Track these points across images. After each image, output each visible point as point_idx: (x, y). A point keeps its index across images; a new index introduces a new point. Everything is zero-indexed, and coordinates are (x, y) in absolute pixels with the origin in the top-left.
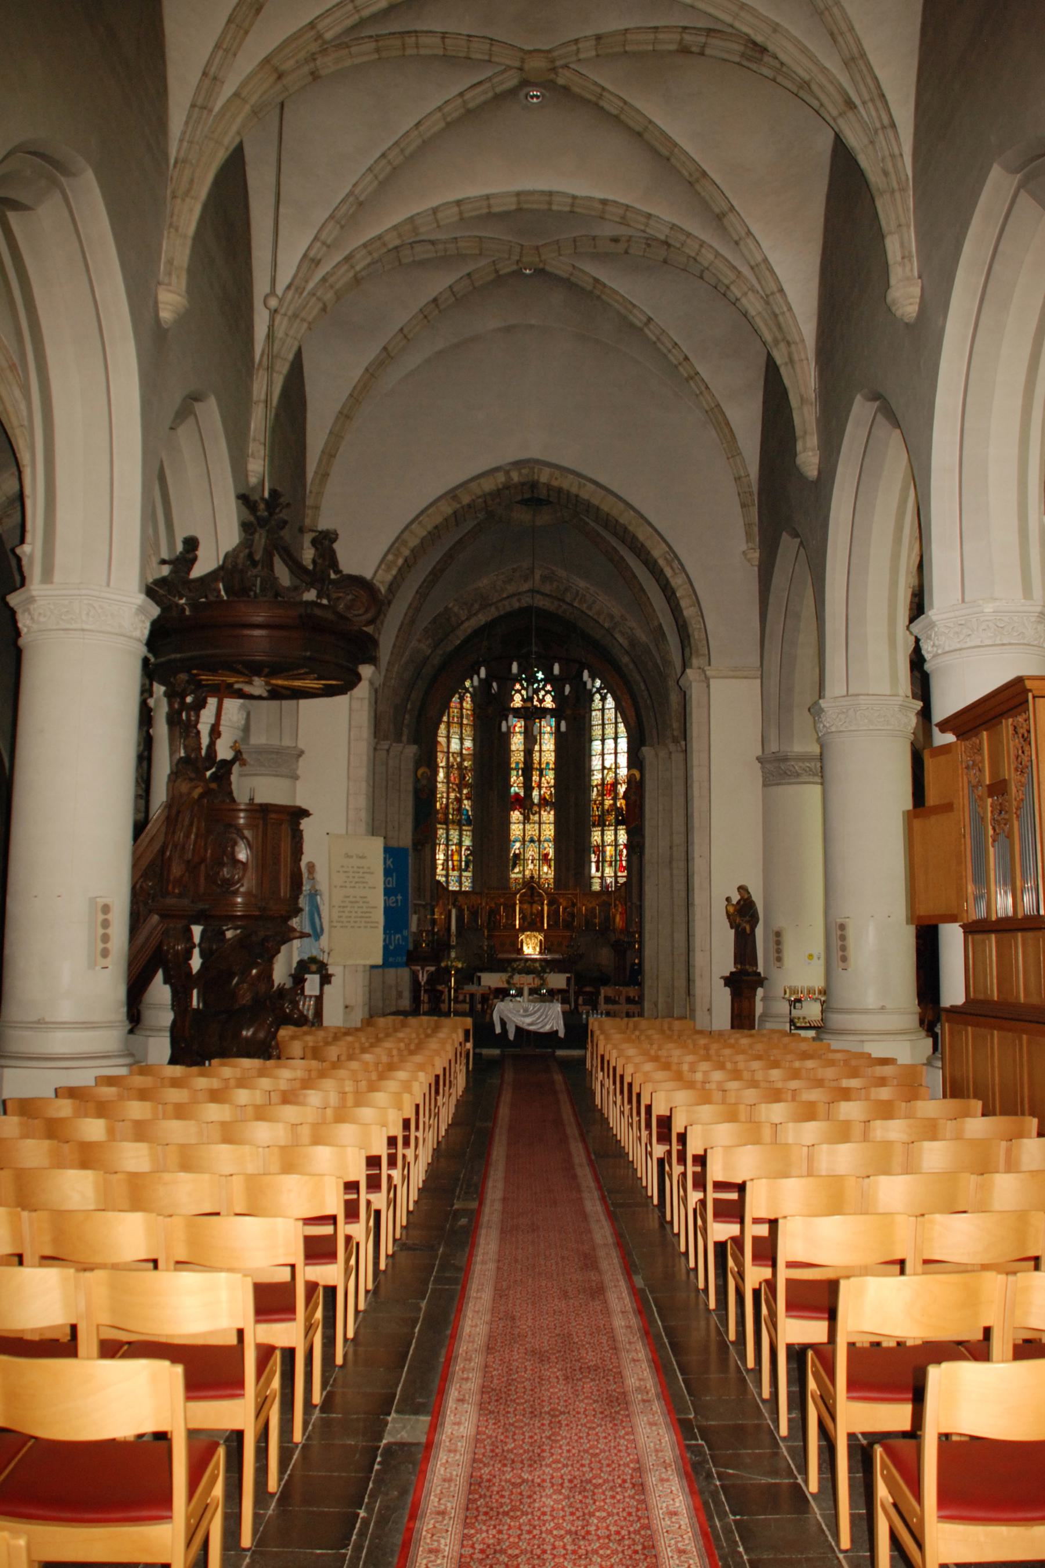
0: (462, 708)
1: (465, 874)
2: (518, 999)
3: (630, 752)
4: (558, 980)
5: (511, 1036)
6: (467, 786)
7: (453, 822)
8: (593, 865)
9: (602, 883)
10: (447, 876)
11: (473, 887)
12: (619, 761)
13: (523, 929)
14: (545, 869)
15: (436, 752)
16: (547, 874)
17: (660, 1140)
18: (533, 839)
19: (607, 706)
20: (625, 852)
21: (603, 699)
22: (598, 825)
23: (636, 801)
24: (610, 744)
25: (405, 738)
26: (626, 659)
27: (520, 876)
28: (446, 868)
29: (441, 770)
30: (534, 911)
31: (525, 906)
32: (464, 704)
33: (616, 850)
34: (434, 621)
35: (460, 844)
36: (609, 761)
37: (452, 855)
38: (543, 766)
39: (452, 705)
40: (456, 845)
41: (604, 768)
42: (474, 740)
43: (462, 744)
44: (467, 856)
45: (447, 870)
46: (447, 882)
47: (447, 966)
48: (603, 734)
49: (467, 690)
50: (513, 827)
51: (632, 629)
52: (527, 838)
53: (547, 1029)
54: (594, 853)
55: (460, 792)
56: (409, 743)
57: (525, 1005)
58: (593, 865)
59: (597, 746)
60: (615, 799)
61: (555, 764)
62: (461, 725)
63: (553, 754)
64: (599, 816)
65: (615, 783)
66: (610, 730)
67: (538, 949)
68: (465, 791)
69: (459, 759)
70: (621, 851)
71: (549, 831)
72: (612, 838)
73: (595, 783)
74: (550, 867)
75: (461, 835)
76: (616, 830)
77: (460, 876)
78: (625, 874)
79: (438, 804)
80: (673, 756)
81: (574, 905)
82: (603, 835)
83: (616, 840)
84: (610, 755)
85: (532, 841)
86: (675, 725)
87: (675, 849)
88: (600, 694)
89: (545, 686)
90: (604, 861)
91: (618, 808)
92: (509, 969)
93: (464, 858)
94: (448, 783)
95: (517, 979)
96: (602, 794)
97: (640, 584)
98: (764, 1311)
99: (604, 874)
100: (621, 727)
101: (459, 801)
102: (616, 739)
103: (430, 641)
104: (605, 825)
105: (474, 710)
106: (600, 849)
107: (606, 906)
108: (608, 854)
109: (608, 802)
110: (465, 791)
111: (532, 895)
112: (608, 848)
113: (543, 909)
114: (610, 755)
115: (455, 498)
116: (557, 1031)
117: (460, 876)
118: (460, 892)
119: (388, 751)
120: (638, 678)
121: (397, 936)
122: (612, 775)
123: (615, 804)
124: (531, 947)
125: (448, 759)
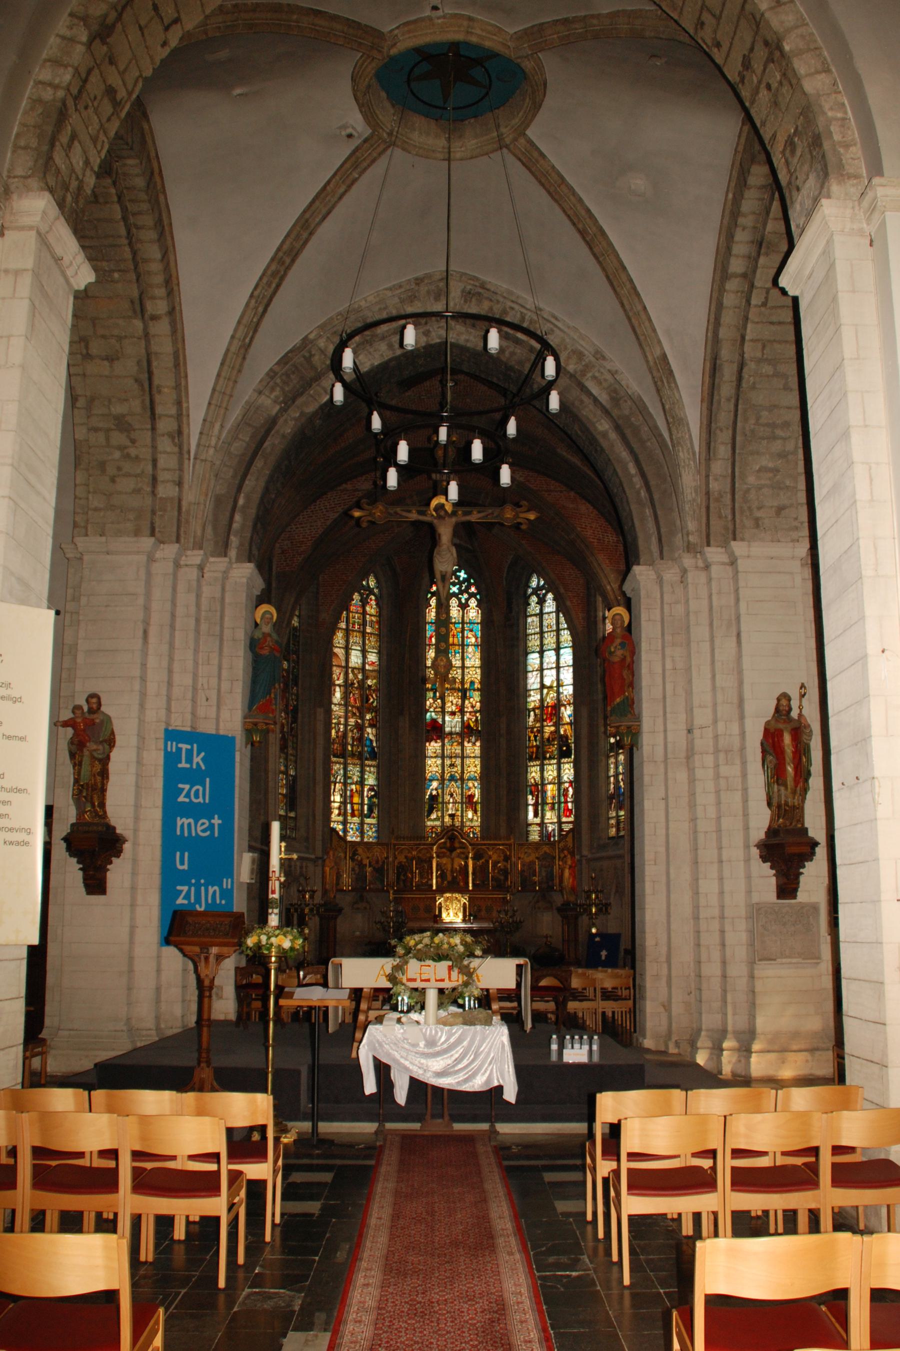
0: (364, 613)
1: (368, 821)
2: (414, 1016)
4: (498, 973)
5: (401, 1095)
6: (369, 710)
7: (353, 755)
8: (531, 809)
9: (541, 832)
10: (345, 823)
11: (378, 838)
12: (562, 677)
13: (441, 891)
14: (470, 814)
15: (331, 666)
16: (471, 820)
17: (606, 1154)
18: (453, 769)
19: (546, 610)
20: (571, 791)
21: (541, 602)
22: (537, 759)
23: (624, 659)
24: (550, 657)
25: (233, 553)
26: (603, 426)
27: (438, 823)
28: (343, 813)
29: (338, 689)
30: (456, 866)
31: (444, 861)
32: (368, 609)
33: (559, 789)
34: (284, 360)
35: (362, 783)
36: (550, 678)
37: (352, 796)
38: (467, 686)
39: (352, 608)
40: (356, 783)
41: (543, 686)
42: (379, 653)
43: (364, 657)
44: (370, 798)
45: (345, 815)
46: (345, 831)
47: (259, 946)
48: (542, 645)
49: (371, 592)
50: (429, 762)
51: (613, 373)
52: (447, 776)
53: (478, 1084)
54: (532, 793)
55: (362, 717)
56: (239, 560)
57: (431, 1029)
59: (533, 659)
60: (557, 725)
61: (480, 683)
62: (364, 634)
63: (479, 671)
64: (537, 746)
65: (558, 705)
66: (550, 640)
67: (461, 915)
68: (368, 717)
69: (360, 676)
70: (566, 790)
71: (474, 767)
72: (556, 775)
73: (532, 706)
74: (475, 812)
75: (362, 772)
76: (559, 764)
77: (362, 824)
78: (571, 819)
79: (333, 732)
80: (690, 576)
81: (507, 859)
82: (542, 771)
83: (559, 776)
84: (551, 670)
85: (452, 778)
86: (691, 525)
87: (697, 733)
88: (538, 596)
89: (468, 587)
90: (544, 803)
91: (561, 737)
92: (400, 950)
93: (366, 801)
94: (346, 705)
95: (414, 967)
96: (540, 719)
97: (631, 281)
99: (544, 820)
100: (566, 636)
101: (360, 728)
102: (557, 650)
103: (277, 392)
104: (545, 758)
105: (380, 615)
106: (539, 789)
107: (547, 860)
108: (549, 794)
109: (549, 729)
110: (368, 717)
111: (452, 843)
112: (549, 787)
113: (467, 865)
114: (551, 670)
116: (499, 1089)
117: (362, 824)
118: (362, 843)
119: (201, 568)
120: (625, 455)
121: (211, 890)
122: (553, 694)
123: (557, 731)
124: (453, 913)
125: (346, 674)
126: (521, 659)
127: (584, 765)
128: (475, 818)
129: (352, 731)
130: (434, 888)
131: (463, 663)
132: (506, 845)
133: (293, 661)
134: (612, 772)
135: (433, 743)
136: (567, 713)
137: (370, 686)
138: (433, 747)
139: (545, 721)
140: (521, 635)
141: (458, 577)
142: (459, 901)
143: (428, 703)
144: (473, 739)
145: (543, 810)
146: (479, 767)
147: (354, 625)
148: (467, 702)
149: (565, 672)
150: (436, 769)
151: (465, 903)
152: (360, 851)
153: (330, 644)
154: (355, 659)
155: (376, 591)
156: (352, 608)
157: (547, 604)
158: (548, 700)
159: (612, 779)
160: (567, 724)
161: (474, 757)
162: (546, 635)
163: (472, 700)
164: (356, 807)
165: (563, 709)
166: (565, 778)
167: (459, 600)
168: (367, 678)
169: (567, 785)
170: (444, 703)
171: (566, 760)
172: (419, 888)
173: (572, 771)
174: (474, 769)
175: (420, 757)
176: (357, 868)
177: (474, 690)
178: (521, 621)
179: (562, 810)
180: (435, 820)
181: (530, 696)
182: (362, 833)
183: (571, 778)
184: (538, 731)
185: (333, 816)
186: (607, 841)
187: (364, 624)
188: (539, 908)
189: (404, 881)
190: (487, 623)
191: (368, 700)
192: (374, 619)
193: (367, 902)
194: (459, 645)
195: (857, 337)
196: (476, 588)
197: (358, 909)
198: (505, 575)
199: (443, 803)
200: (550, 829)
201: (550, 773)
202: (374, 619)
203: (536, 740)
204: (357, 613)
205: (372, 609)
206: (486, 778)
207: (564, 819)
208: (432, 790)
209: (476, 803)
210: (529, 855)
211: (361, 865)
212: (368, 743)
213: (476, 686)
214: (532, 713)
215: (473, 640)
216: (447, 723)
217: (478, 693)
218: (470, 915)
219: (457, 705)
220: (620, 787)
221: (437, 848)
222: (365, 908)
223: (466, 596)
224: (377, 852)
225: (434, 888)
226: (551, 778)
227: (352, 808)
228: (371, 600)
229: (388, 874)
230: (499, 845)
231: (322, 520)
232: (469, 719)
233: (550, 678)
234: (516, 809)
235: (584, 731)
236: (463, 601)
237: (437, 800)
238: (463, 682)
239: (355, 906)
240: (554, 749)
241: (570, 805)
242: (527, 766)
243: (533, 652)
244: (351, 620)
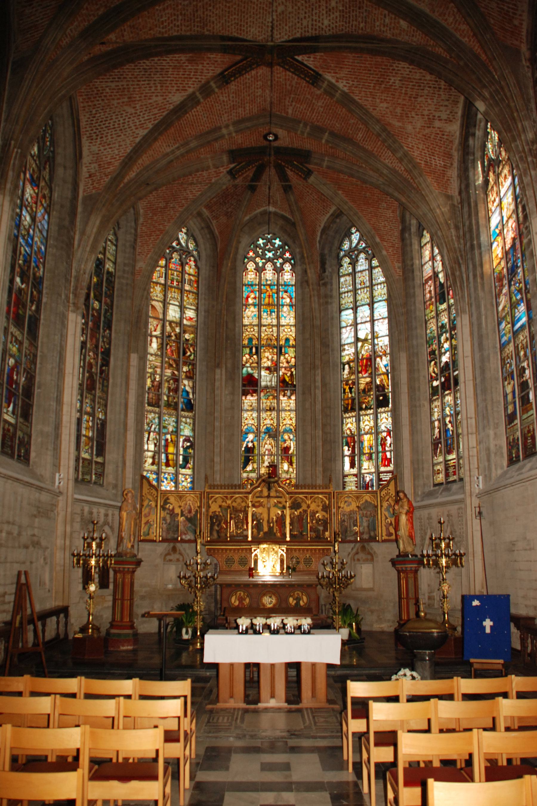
0: (183, 272)
3: (392, 318)
8: (347, 460)
12: (376, 329)
13: (257, 541)
14: (286, 466)
16: (287, 472)
19: (359, 268)
21: (354, 263)
22: (353, 410)
24: (364, 312)
29: (154, 340)
31: (260, 510)
32: (187, 268)
35: (177, 432)
36: (364, 331)
37: (166, 446)
38: (282, 342)
41: (357, 339)
42: (197, 310)
43: (182, 312)
44: (186, 449)
46: (158, 480)
48: (355, 301)
49: (188, 253)
52: (263, 429)
54: (348, 444)
59: (347, 316)
61: (295, 340)
63: (293, 329)
64: (353, 399)
66: (363, 296)
69: (178, 330)
70: (384, 439)
71: (289, 420)
73: (346, 359)
74: (291, 464)
78: (391, 468)
82: (358, 421)
83: (376, 425)
90: (361, 453)
91: (377, 387)
99: (359, 471)
102: (371, 305)
104: (361, 409)
106: (354, 441)
108: (366, 444)
110: (185, 369)
112: (366, 437)
115: (202, 228)
117: (177, 474)
122: (368, 347)
125: (163, 327)
126: (336, 315)
127: (405, 412)
128: (291, 470)
129: (169, 382)
130: (250, 539)
131: (278, 322)
132: (326, 493)
133: (106, 303)
134: (436, 416)
135: (249, 397)
136: (383, 363)
137: (187, 340)
138: (250, 400)
139: (361, 372)
140: (335, 293)
141: (273, 245)
142: (276, 553)
143: (244, 359)
144: (289, 393)
145: (360, 460)
146: (294, 420)
147: (172, 281)
148: (282, 358)
149: (380, 324)
150: (252, 422)
151: (282, 555)
152: (172, 499)
153: (148, 298)
154: (173, 313)
155: (195, 253)
156: (171, 265)
157: (359, 263)
158: (363, 352)
159: (436, 423)
160: (383, 374)
161: (289, 411)
162: (359, 292)
163: (287, 355)
164: (170, 457)
165: (378, 359)
166: (383, 428)
167: (274, 264)
168: (185, 332)
169: (384, 434)
170: (260, 359)
171: (383, 409)
172: (234, 540)
173: (390, 419)
174: (289, 422)
175: (236, 410)
176: (168, 517)
177: (289, 347)
178: (334, 281)
180: (251, 471)
181: (344, 350)
182: (176, 483)
183: (390, 426)
184: (353, 383)
185: (146, 465)
186: (432, 488)
187: (182, 281)
188: (358, 560)
189: (218, 532)
190: (302, 283)
191: (185, 353)
192: (193, 278)
193: (181, 554)
195: (162, 698)
196: (290, 254)
197: (171, 560)
198: (318, 238)
199: (259, 454)
200: (368, 479)
201: (367, 423)
202: (193, 278)
203: (351, 392)
204: (176, 271)
205: (191, 269)
206: (300, 430)
207: (382, 469)
208: (248, 442)
210: (349, 504)
211: (172, 513)
213: (291, 343)
214: (347, 367)
215: (288, 300)
216: (263, 377)
217: (292, 350)
218: (288, 568)
219: (272, 360)
220: (447, 431)
221: (253, 497)
222: (178, 560)
223: (281, 261)
224: (192, 502)
225: (250, 539)
226: (367, 428)
227: (167, 457)
228: (190, 261)
229: (200, 524)
230: (318, 493)
231: (131, 139)
232: (284, 374)
233: (364, 331)
234: (331, 459)
235: (404, 377)
236: (278, 265)
237: (253, 452)
238: (278, 339)
239: (168, 558)
240: (371, 399)
241: (388, 454)
242: (342, 418)
243: (347, 309)
244: (170, 277)
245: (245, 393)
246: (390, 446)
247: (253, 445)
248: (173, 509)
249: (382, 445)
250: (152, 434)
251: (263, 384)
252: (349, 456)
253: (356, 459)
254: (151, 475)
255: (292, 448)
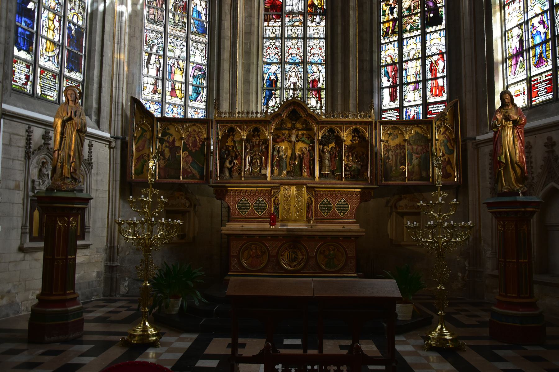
8: (386, 94)
33: (424, 65)
58: (386, 94)
64: (394, 20)
71: (318, 51)
74: (319, 98)
98: (339, 30)
138: (272, 27)
146: (324, 50)
161: (318, 38)
164: (178, 86)
169: (435, 58)
176: (167, 151)
179: (429, 89)
185: (147, 91)
189: (230, 170)
194: (300, 89)
207: (430, 100)
209: (320, 89)
212: (195, 15)
245: (267, 19)
246: (443, 71)
247: (277, 77)
248: (174, 141)
249: (431, 71)
250: (153, 57)
251: (288, 9)
252: (389, 87)
253: (398, 91)
254: (151, 106)
255: (321, 81)
